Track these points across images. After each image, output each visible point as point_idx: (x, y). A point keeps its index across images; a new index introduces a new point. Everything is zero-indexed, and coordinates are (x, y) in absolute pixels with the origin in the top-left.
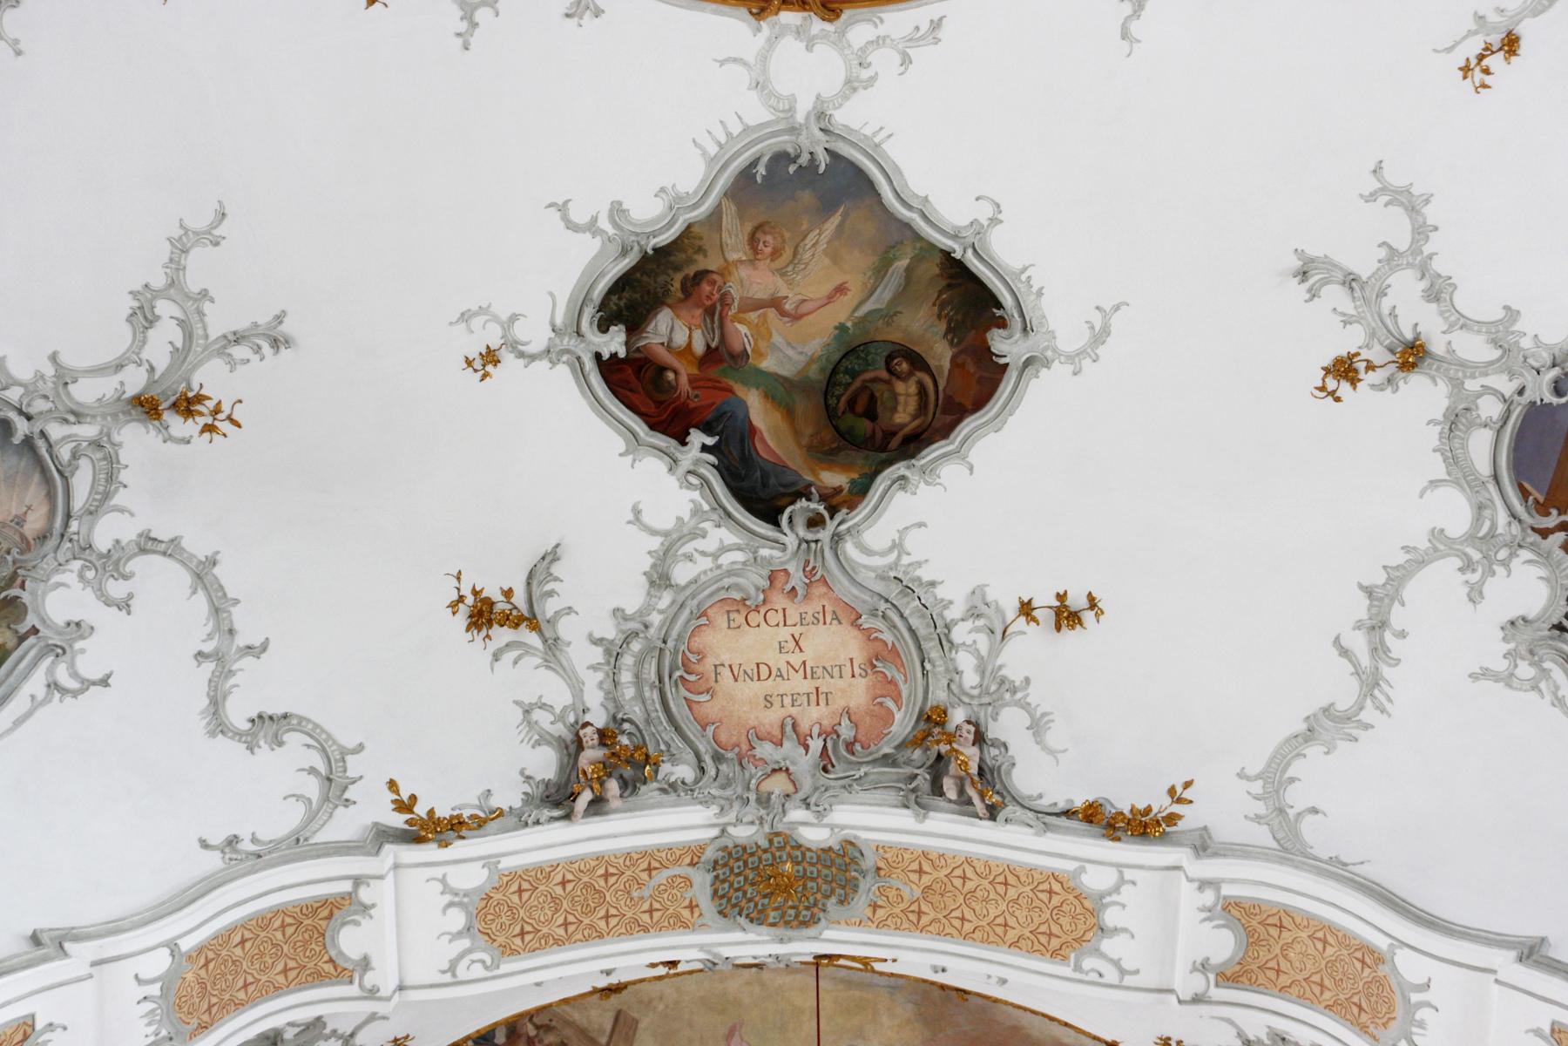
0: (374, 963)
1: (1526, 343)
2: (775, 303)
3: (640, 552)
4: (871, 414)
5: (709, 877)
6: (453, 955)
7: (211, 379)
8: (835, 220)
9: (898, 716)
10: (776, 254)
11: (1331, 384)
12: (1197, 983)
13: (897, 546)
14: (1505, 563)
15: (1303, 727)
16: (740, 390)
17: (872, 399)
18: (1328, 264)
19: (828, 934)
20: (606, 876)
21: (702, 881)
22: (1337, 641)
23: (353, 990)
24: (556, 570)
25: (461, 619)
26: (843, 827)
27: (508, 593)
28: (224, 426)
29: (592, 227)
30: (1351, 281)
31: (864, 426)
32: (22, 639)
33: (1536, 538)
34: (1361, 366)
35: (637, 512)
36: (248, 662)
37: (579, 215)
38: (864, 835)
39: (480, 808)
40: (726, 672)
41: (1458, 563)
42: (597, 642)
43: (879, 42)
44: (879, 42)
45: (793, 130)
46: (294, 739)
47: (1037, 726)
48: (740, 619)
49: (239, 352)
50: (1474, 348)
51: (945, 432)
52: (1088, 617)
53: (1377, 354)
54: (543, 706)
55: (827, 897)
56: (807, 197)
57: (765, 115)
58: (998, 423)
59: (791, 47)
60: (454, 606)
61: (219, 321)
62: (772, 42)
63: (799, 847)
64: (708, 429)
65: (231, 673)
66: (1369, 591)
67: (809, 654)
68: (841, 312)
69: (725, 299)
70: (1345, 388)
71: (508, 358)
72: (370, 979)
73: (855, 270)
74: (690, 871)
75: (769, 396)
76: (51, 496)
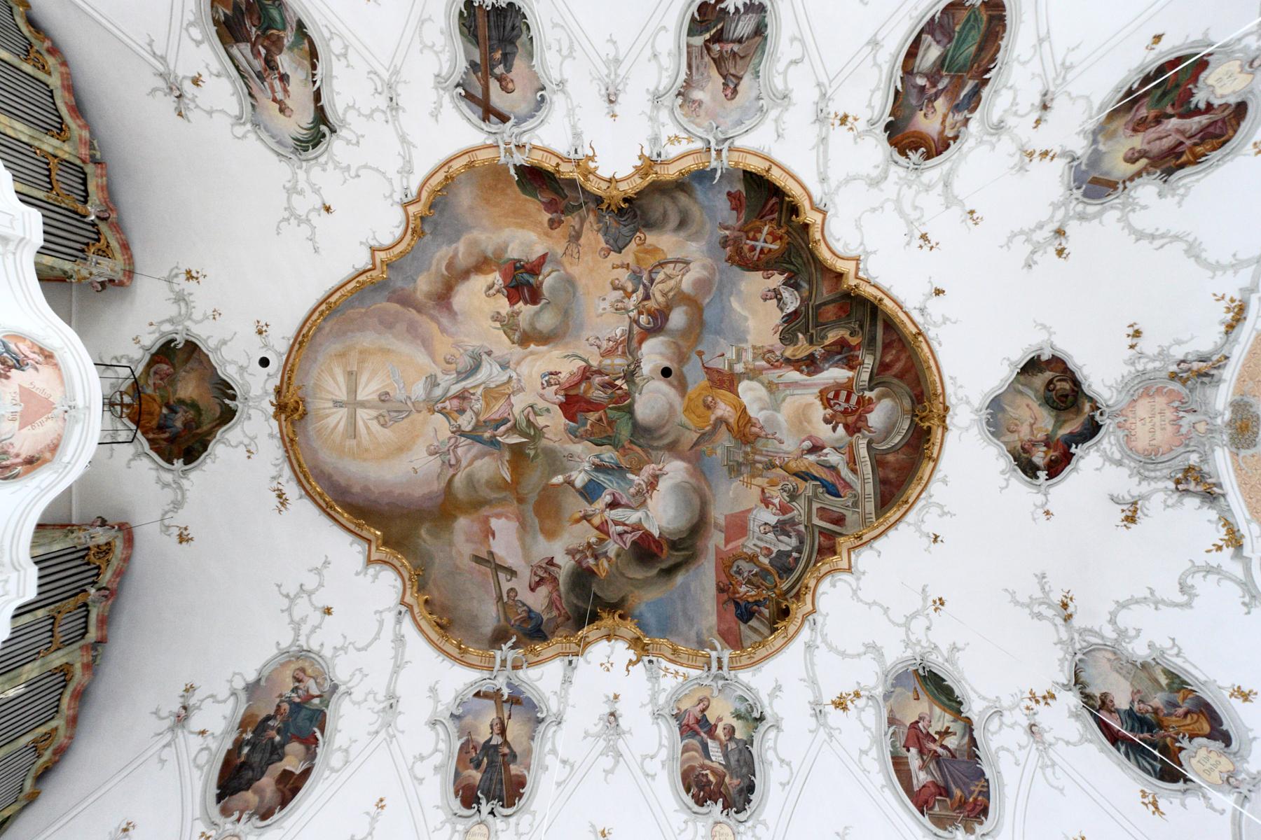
1: (1061, 199)
2: (1031, 425)
3: (1111, 469)
4: (1066, 396)
5: (1242, 450)
7: (1057, 598)
8: (1008, 408)
9: (1170, 387)
10: (1017, 425)
11: (1064, 255)
13: (1110, 388)
14: (1134, 199)
15: (1193, 259)
16: (1058, 436)
17: (1062, 396)
18: (1027, 260)
21: (1243, 452)
22: (1157, 249)
24: (1115, 495)
25: (1133, 526)
27: (1123, 511)
28: (1070, 595)
29: (1007, 480)
30: (1033, 252)
31: (1070, 398)
32: (1158, 663)
33: (1126, 191)
34: (1060, 247)
35: (1097, 469)
36: (1156, 594)
37: (1004, 484)
39: (1217, 524)
40: (1152, 443)
41: (1131, 214)
42: (1140, 483)
43: (956, 395)
44: (956, 395)
45: (981, 420)
46: (1190, 581)
47: (1179, 343)
48: (1133, 438)
49: (1047, 588)
50: (1060, 214)
51: (1072, 373)
52: (1136, 327)
53: (1057, 242)
54: (1165, 501)
56: (1000, 415)
57: (976, 428)
58: (1070, 357)
59: (956, 420)
60: (1128, 528)
61: (1038, 594)
62: (955, 426)
64: (1070, 447)
65: (1163, 600)
66: (1137, 240)
68: (1035, 405)
69: (1030, 441)
70: (1066, 251)
71: (1047, 508)
73: (1020, 400)
75: (1060, 427)
76: (1099, 649)
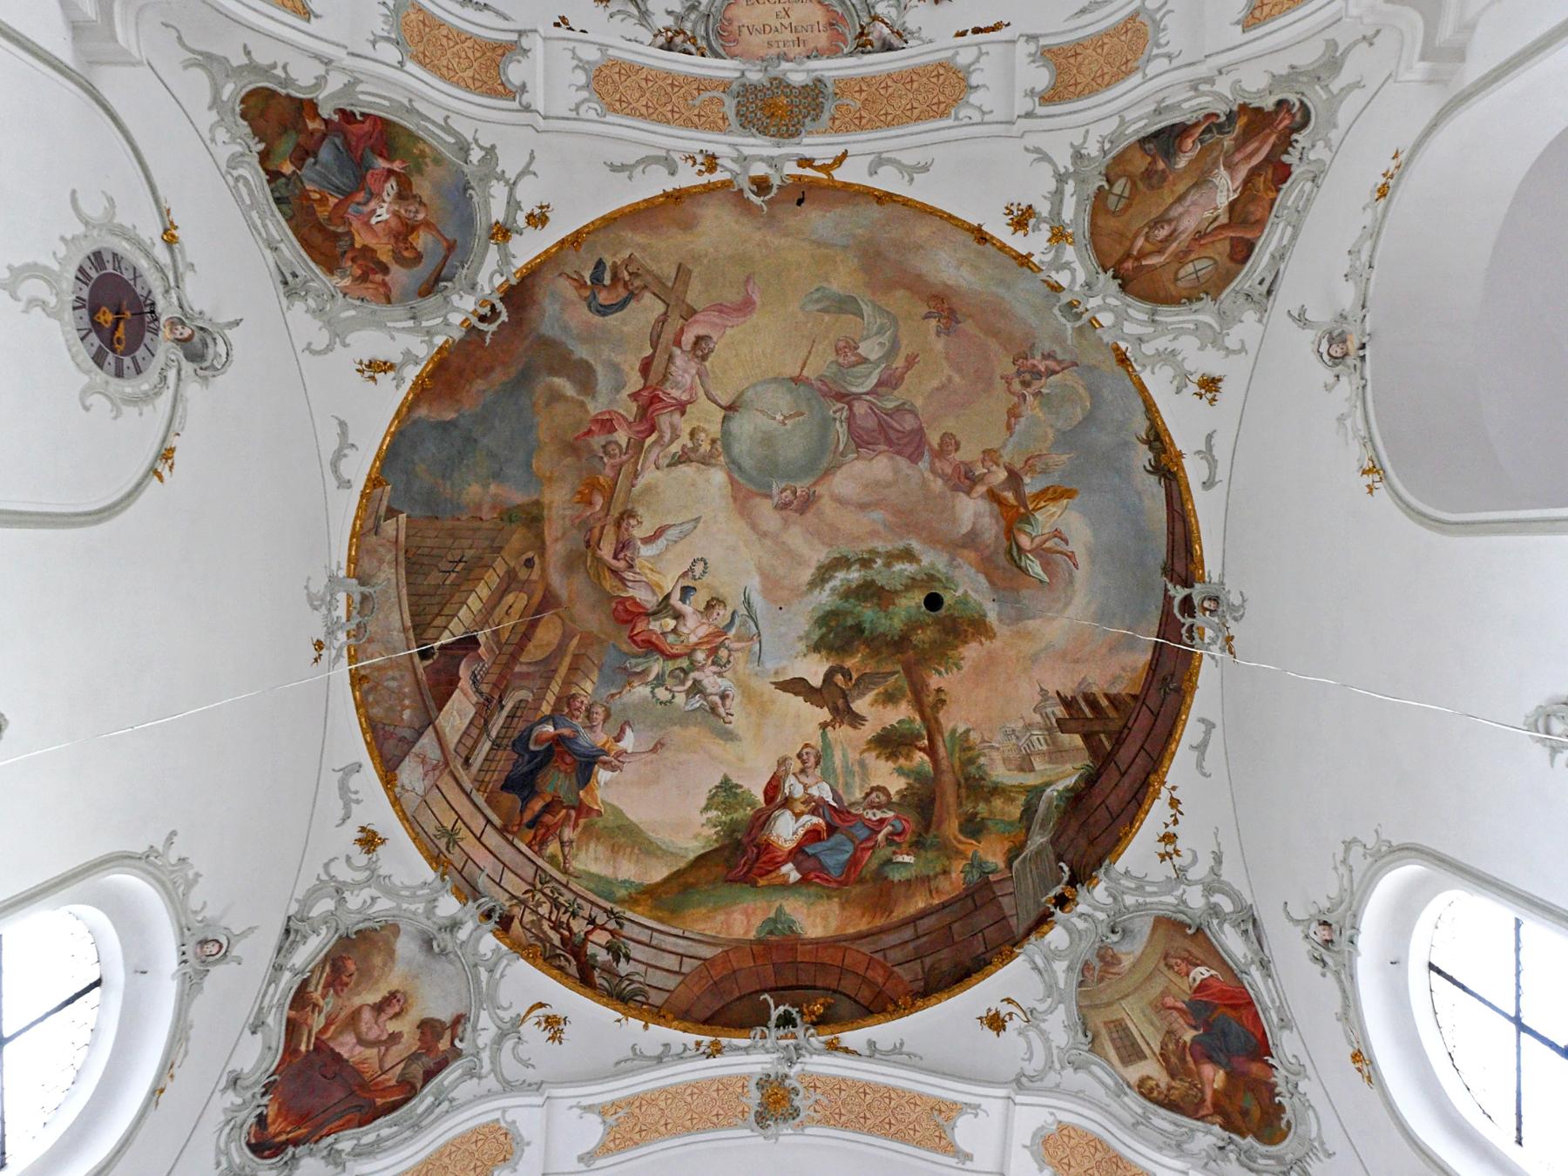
0: (528, 88)
6: (577, 100)
12: (1029, 104)
19: (806, 140)
20: (672, 85)
23: (515, 105)
26: (814, 71)
38: (826, 74)
40: (745, 30)
42: (670, 13)
55: (805, 117)
63: (788, 86)
67: (793, 19)
72: (526, 98)
74: (723, 96)
